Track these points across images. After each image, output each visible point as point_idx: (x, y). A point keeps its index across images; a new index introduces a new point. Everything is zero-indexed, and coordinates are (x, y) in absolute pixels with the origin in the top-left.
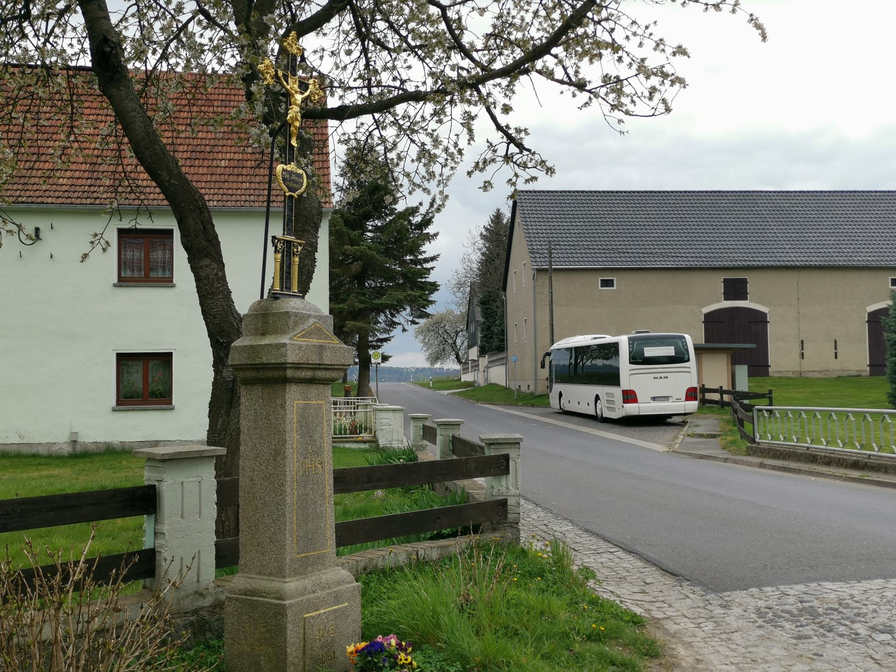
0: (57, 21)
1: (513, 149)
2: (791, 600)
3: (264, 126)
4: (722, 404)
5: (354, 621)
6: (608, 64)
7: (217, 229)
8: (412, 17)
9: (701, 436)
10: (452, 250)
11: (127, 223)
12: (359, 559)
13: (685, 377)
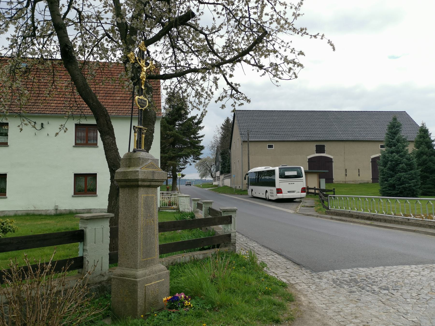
0: (48, 38)
1: (234, 92)
2: (347, 275)
3: (131, 81)
4: (315, 194)
6: (272, 58)
7: (113, 124)
8: (193, 38)
9: (307, 207)
10: (210, 133)
11: (77, 122)
12: (169, 259)
13: (301, 183)
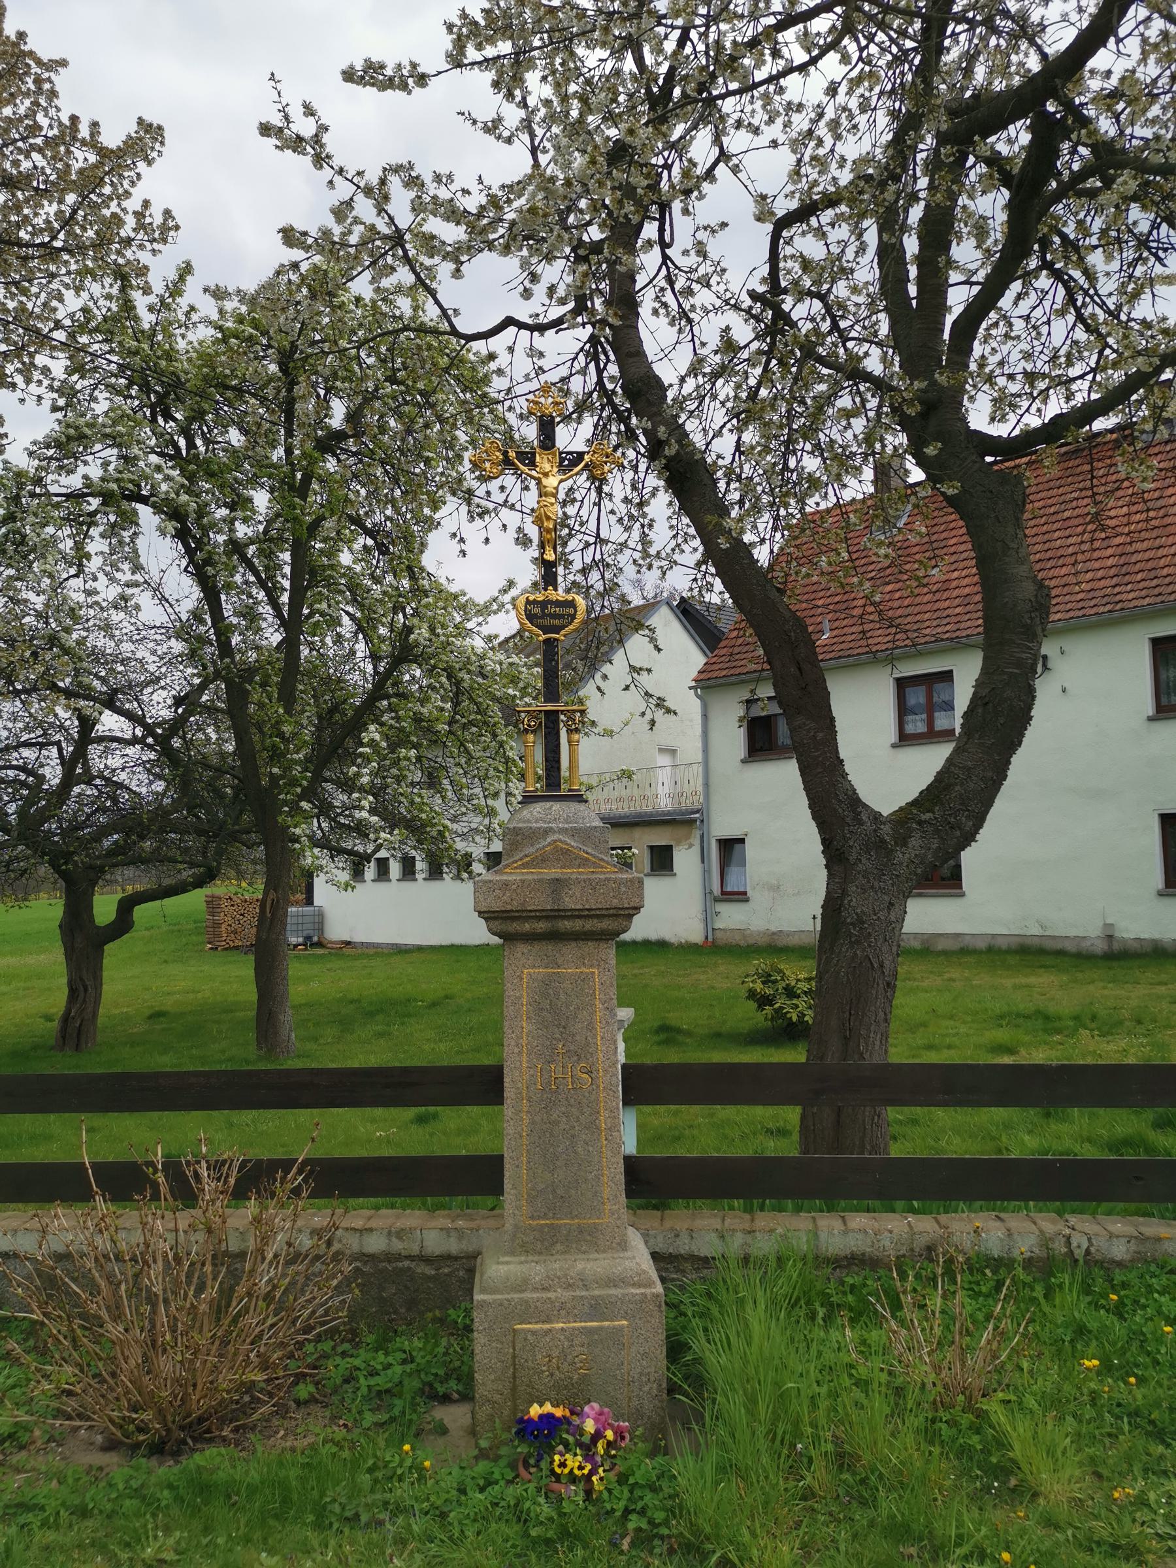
5: (645, 1355)
